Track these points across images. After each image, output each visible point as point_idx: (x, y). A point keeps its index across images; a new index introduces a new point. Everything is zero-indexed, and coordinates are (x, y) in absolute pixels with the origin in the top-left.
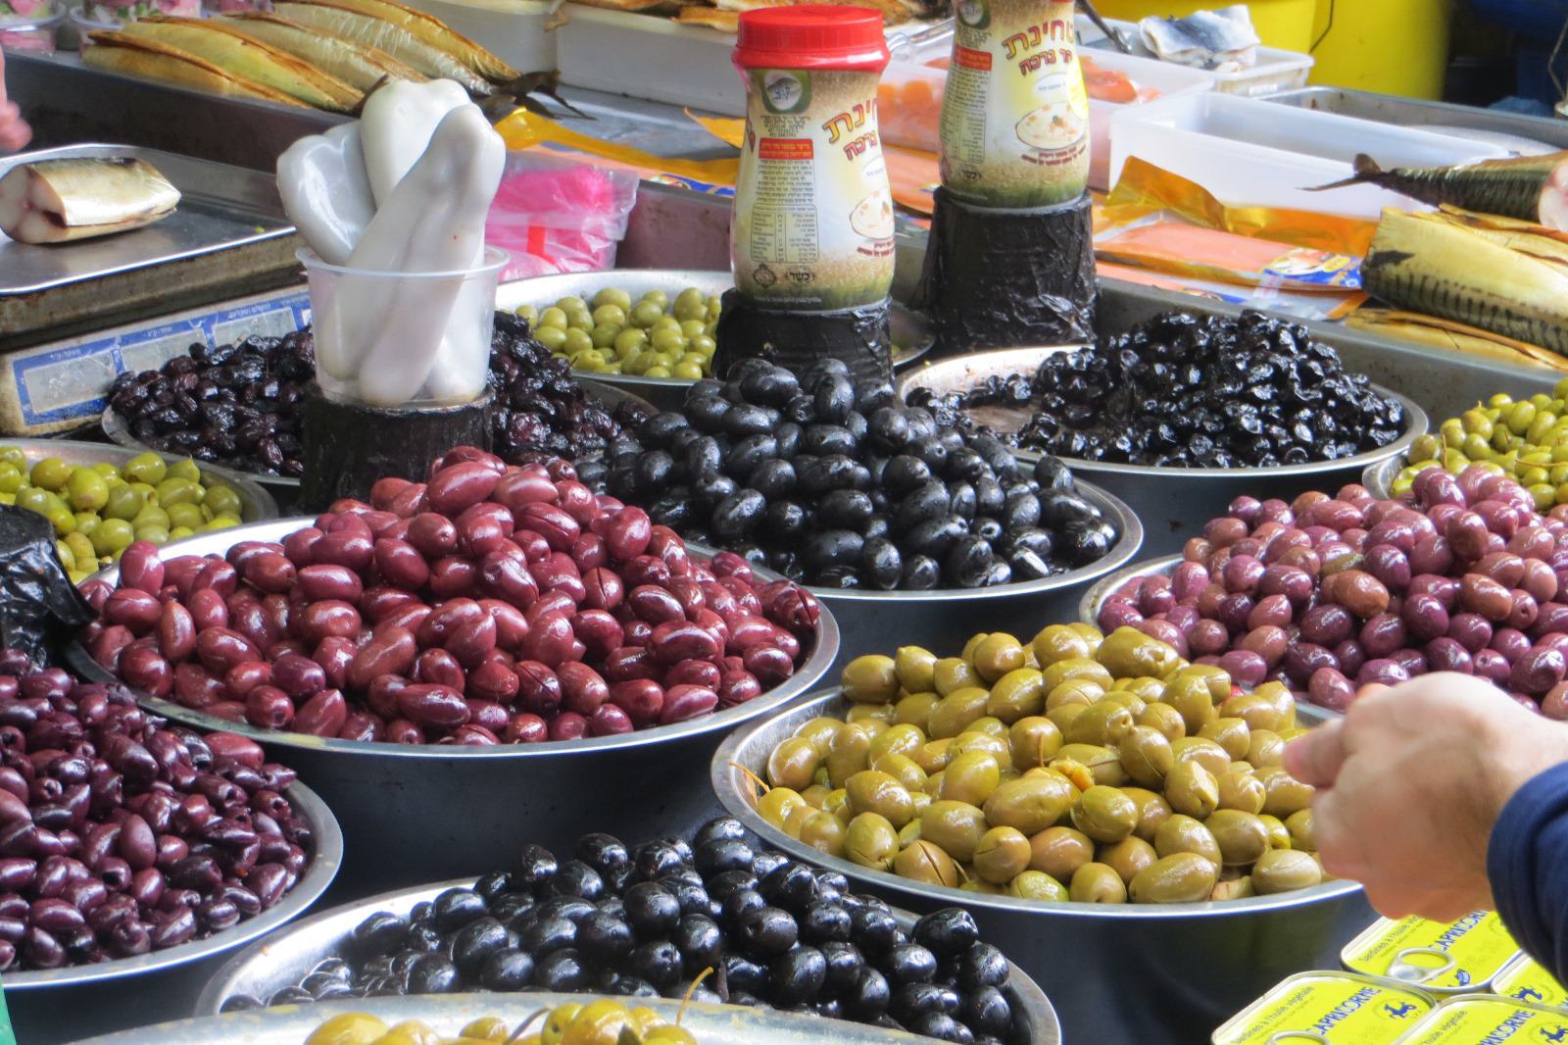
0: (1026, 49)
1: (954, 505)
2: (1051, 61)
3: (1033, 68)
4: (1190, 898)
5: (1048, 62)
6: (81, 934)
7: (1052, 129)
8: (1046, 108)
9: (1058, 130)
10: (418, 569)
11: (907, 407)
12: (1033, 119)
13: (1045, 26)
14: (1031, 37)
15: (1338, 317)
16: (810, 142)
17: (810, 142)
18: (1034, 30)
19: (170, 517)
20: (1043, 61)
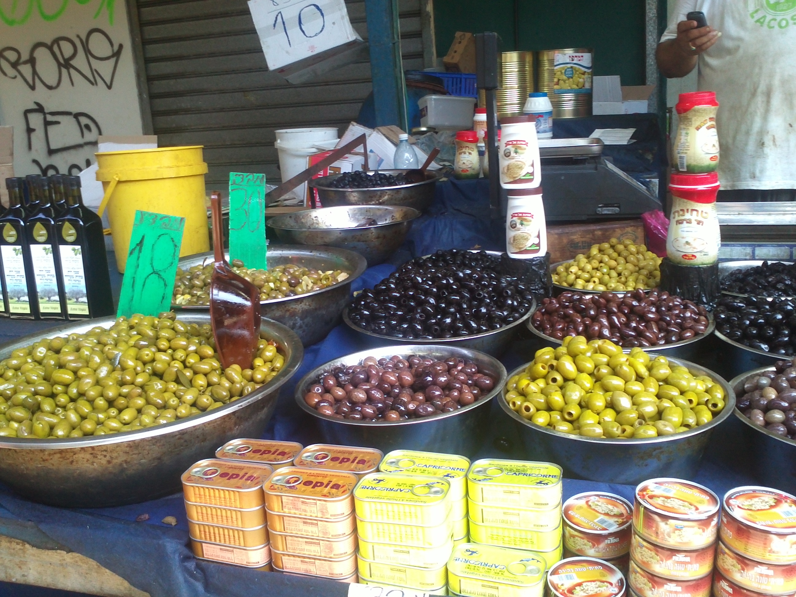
0: (679, 216)
1: (263, 546)
2: (689, 222)
3: (680, 223)
4: (694, 582)
5: (687, 223)
6: (786, 337)
7: (685, 245)
8: (683, 238)
9: (688, 246)
10: (464, 386)
11: (549, 364)
12: (677, 240)
13: (688, 210)
14: (681, 213)
15: (566, 397)
16: (340, 168)
17: (340, 168)
18: (682, 210)
19: (70, 370)
20: (685, 222)
